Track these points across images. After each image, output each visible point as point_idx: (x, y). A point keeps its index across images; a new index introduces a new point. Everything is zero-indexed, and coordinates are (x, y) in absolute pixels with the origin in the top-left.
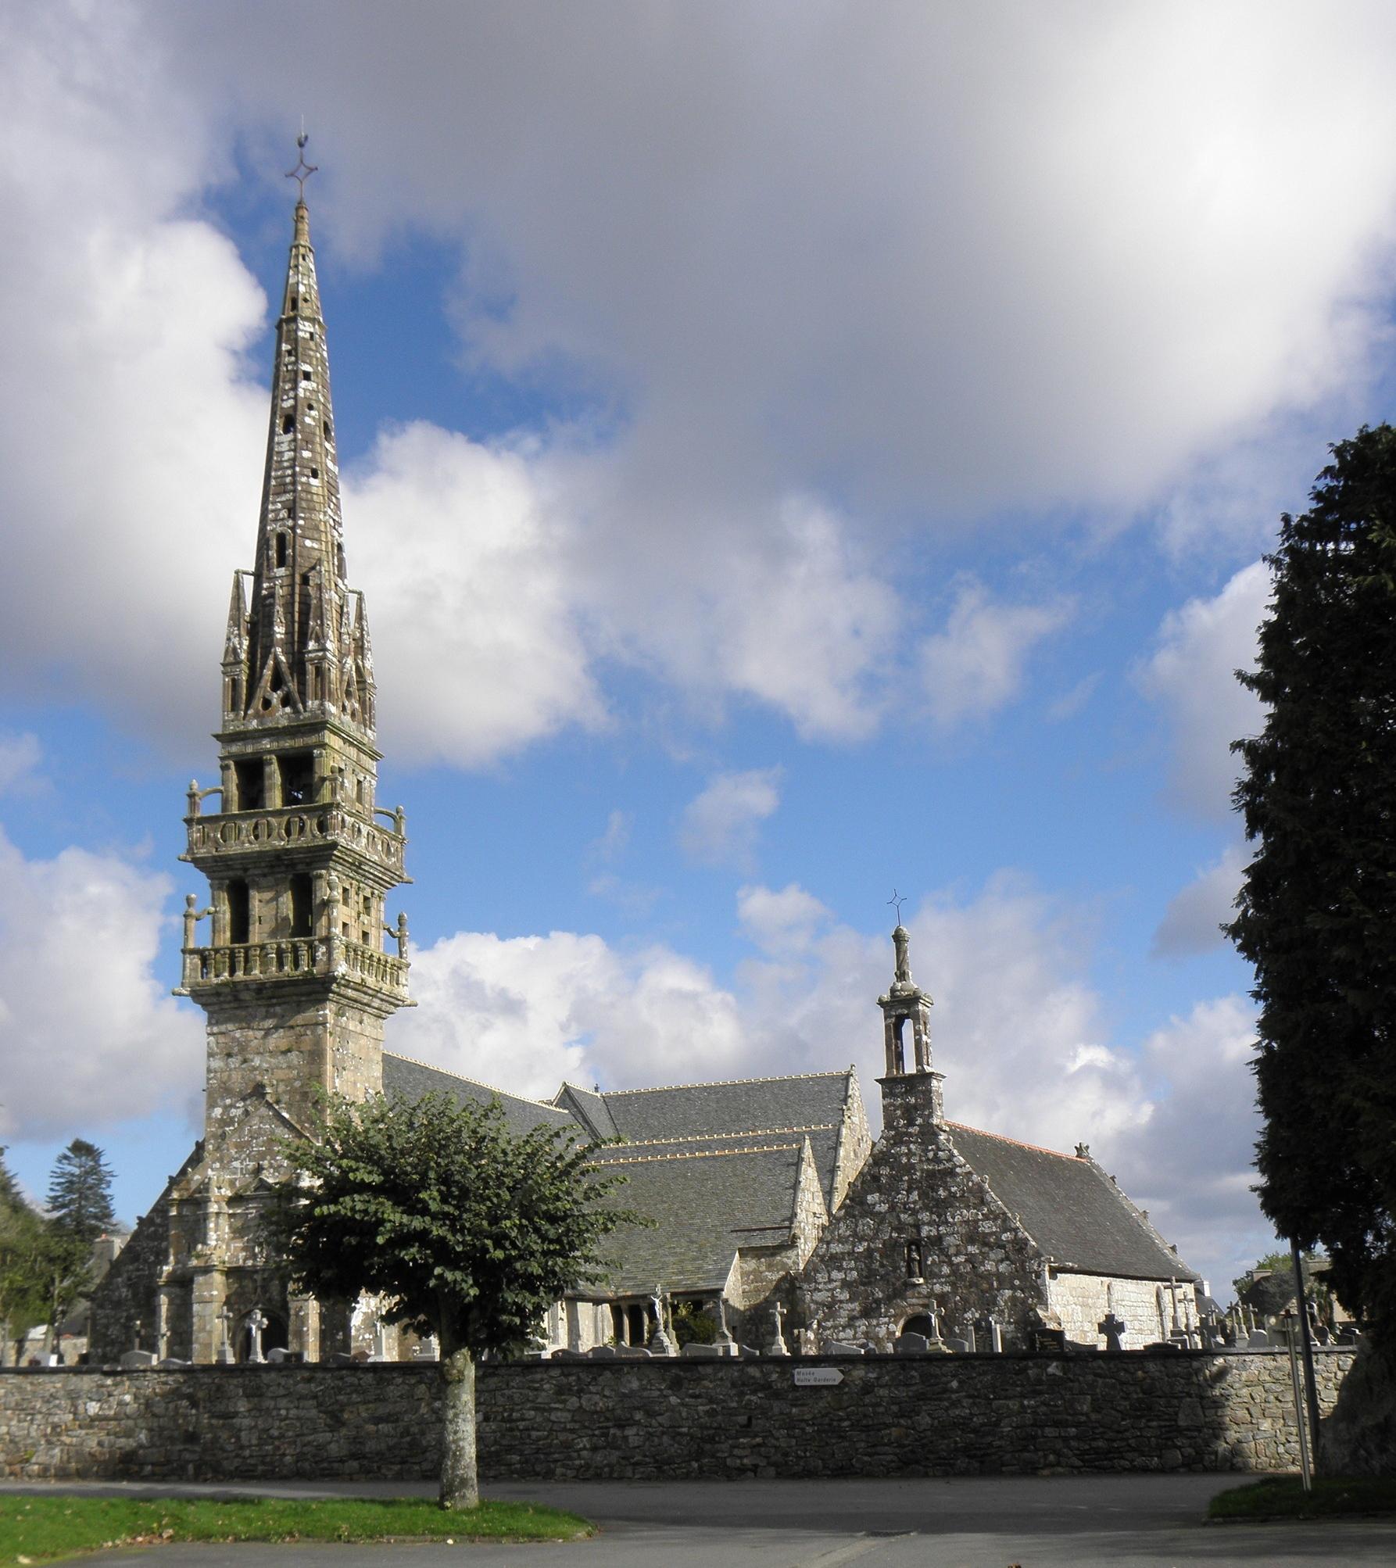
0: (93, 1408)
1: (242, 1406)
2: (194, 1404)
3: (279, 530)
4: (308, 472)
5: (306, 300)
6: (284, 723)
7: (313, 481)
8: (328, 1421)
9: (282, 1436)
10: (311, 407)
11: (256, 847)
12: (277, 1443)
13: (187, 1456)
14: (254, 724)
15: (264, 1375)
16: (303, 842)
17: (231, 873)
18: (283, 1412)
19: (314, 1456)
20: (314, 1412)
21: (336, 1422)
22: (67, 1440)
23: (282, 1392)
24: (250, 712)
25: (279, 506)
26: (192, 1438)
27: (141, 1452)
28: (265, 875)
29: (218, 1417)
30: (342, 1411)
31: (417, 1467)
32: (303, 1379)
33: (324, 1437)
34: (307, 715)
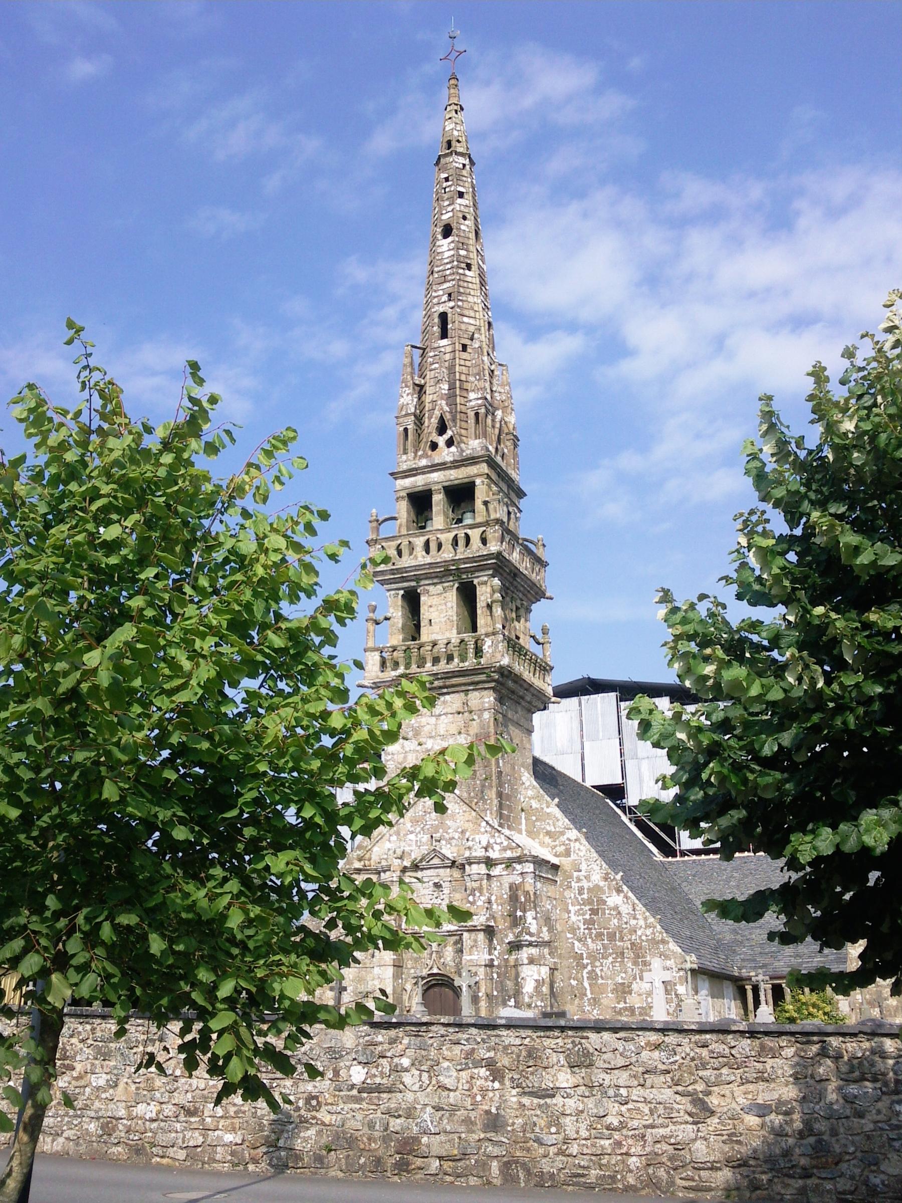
0: (358, 1074)
1: (565, 1079)
2: (497, 1074)
3: (441, 310)
4: (464, 265)
5: (458, 141)
6: (449, 459)
7: (467, 272)
8: (690, 1108)
9: (623, 1126)
10: (465, 218)
11: (428, 560)
12: (617, 1136)
13: (491, 1149)
14: (424, 462)
15: (593, 1036)
16: (468, 554)
17: (406, 584)
18: (623, 1091)
19: (671, 1159)
20: (667, 1094)
21: (702, 1110)
22: (327, 1119)
23: (621, 1062)
24: (420, 453)
25: (441, 293)
26: (494, 1122)
27: (425, 1140)
28: (434, 584)
29: (532, 1094)
30: (708, 1094)
31: (829, 1186)
32: (648, 1044)
33: (685, 1132)
34: (468, 452)
